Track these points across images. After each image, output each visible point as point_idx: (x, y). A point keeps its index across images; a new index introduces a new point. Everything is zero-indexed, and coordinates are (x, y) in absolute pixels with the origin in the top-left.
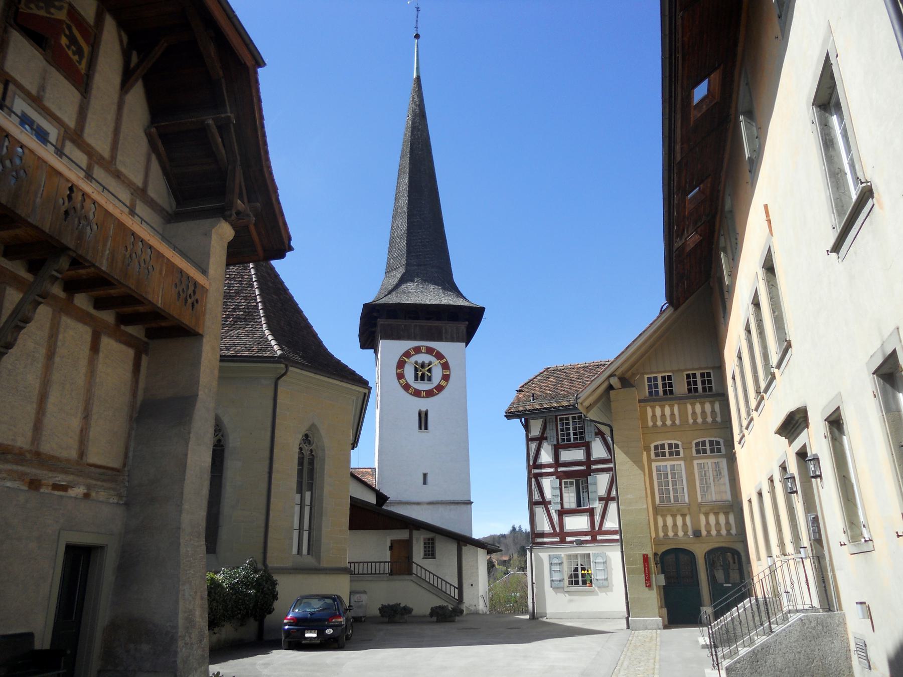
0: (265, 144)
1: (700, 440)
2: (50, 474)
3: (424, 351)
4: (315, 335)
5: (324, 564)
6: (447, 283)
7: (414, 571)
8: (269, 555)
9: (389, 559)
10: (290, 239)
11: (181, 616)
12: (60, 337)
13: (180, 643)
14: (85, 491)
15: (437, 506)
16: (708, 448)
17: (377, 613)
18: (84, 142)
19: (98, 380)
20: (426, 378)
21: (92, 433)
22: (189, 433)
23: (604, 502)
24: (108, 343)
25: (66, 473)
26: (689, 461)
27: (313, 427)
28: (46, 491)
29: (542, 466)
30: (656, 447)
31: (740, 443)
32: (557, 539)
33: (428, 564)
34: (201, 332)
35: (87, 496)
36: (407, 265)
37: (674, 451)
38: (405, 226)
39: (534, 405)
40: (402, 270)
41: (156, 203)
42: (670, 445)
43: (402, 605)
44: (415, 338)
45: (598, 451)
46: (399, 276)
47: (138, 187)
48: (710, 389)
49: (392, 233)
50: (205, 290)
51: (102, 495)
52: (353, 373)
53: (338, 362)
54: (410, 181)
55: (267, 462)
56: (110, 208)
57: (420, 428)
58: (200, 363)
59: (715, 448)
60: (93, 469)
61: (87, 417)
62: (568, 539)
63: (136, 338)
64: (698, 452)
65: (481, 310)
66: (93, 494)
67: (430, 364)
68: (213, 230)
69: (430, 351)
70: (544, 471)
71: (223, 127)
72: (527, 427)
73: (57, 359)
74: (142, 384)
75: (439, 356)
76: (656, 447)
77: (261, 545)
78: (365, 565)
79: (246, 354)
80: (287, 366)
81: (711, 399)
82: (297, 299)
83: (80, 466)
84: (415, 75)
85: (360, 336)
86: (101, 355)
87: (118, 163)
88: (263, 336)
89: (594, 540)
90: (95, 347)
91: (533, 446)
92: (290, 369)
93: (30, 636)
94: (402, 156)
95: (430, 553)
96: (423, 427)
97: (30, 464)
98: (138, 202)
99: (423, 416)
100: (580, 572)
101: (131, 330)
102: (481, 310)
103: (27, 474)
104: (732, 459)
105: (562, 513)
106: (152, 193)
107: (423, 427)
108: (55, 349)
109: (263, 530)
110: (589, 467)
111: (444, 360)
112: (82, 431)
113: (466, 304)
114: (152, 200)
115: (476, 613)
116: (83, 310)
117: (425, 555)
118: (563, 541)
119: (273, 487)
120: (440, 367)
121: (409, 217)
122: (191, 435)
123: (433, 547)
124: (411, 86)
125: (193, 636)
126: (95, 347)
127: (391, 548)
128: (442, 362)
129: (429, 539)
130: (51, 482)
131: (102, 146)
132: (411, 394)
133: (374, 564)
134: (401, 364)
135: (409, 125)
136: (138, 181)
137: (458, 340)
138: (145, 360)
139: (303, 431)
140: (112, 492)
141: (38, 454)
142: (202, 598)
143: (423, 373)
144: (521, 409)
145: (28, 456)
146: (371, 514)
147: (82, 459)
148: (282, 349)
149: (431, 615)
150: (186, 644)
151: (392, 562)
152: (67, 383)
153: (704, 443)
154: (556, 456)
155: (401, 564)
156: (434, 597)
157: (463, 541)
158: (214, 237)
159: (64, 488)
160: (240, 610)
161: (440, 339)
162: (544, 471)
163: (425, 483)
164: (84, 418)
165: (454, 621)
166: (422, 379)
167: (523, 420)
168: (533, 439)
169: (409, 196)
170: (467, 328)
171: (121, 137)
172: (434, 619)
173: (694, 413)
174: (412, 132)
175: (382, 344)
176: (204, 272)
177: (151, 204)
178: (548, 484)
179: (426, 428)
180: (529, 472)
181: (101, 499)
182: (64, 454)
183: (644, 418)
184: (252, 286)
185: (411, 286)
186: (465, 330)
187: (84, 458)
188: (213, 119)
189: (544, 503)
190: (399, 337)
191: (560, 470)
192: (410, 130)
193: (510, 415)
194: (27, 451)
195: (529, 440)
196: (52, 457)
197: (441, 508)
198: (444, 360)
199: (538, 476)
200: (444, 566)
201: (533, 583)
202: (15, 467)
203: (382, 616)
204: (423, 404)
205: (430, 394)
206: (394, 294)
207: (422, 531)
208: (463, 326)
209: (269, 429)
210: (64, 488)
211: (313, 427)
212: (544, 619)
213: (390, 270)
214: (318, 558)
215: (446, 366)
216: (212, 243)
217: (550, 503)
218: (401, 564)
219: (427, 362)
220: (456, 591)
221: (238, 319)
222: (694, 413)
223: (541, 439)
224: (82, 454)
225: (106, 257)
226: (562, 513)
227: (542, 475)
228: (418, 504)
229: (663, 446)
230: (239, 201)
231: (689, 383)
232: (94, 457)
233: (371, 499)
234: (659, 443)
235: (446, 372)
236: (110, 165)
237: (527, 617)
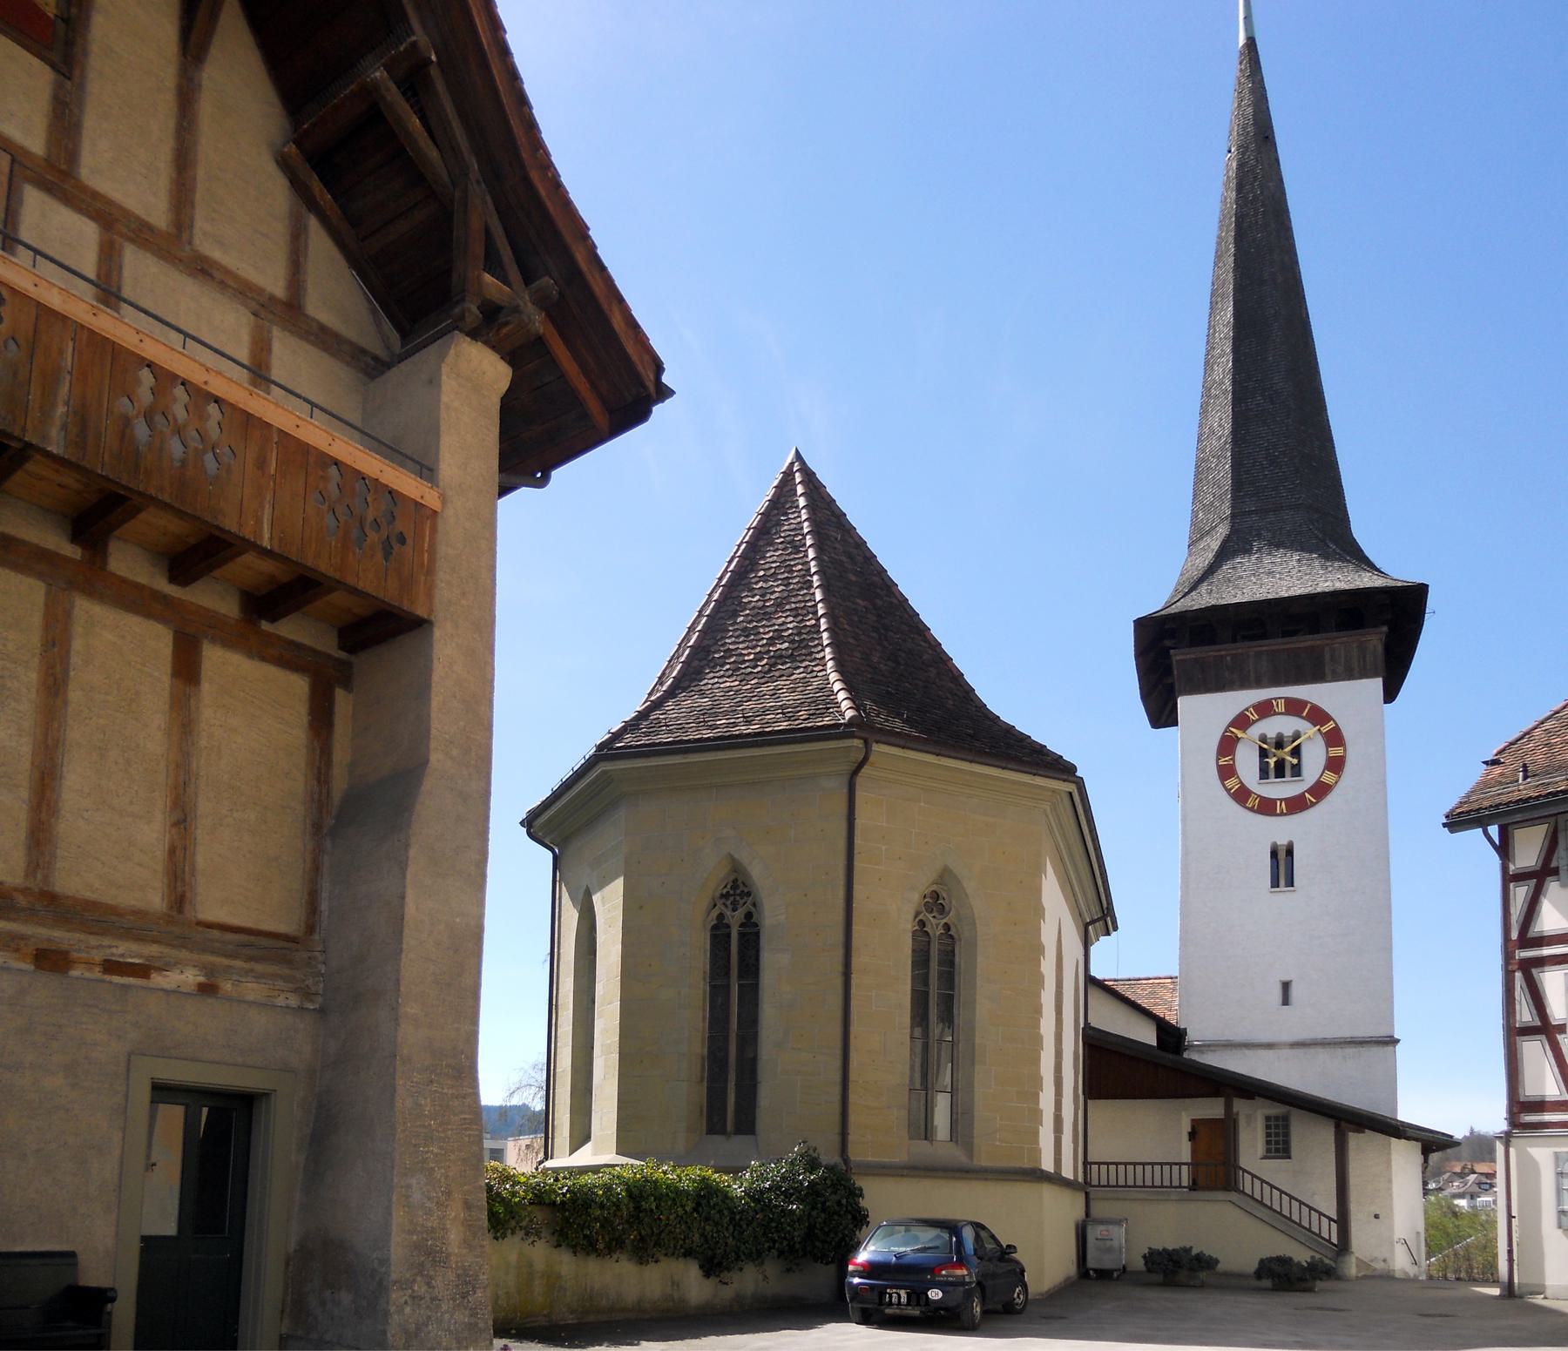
0: (523, 101)
2: (94, 941)
3: (1281, 708)
4: (957, 678)
5: (983, 1160)
6: (1336, 541)
8: (853, 1137)
9: (1186, 1156)
10: (659, 368)
11: (396, 1239)
12: (77, 644)
13: (396, 1296)
15: (1312, 1050)
17: (1139, 1264)
18: (85, 189)
19: (203, 743)
20: (1288, 771)
21: (203, 858)
22: (407, 846)
24: (216, 659)
25: (138, 939)
27: (945, 876)
28: (87, 975)
29: (1542, 941)
33: (1275, 1171)
34: (421, 612)
36: (1233, 516)
38: (1228, 426)
39: (1525, 789)
40: (1223, 530)
41: (337, 336)
43: (1194, 1252)
44: (1258, 683)
46: (1215, 545)
47: (272, 298)
49: (1200, 450)
50: (425, 516)
51: (253, 990)
52: (1040, 750)
53: (1009, 730)
54: (1236, 314)
55: (840, 952)
56: (54, 300)
57: (1275, 883)
58: (428, 687)
60: (216, 933)
61: (182, 818)
63: (314, 651)
65: (1417, 594)
66: (227, 986)
67: (1297, 736)
68: (445, 369)
70: (1547, 951)
71: (414, 82)
72: (1504, 849)
73: (75, 695)
74: (341, 753)
75: (1318, 716)
77: (837, 1118)
78: (1121, 1168)
79: (784, 725)
80: (866, 742)
82: (915, 603)
83: (176, 922)
84: (1242, 40)
85: (1143, 697)
86: (205, 686)
87: (197, 240)
88: (825, 687)
90: (186, 668)
91: (1521, 893)
92: (875, 747)
94: (1219, 256)
95: (1279, 1146)
96: (1282, 882)
97: (45, 923)
98: (276, 332)
99: (1282, 855)
101: (289, 629)
102: (1417, 594)
103: (23, 937)
106: (317, 308)
108: (66, 671)
109: (837, 1089)
111: (1331, 725)
112: (172, 851)
113: (1378, 582)
114: (323, 328)
115: (1388, 1277)
116: (139, 587)
117: (1268, 1151)
119: (853, 1003)
120: (1320, 743)
121: (1236, 402)
122: (412, 853)
124: (1230, 70)
125: (438, 1282)
126: (186, 668)
127: (1192, 1136)
128: (1325, 729)
129: (1277, 1118)
130: (98, 956)
131: (147, 199)
132: (1251, 809)
134: (1227, 745)
135: (1232, 174)
136: (274, 282)
138: (343, 701)
139: (924, 881)
140: (280, 983)
141: (51, 898)
142: (468, 1206)
143: (1280, 760)
144: (1486, 804)
145: (22, 901)
146: (1138, 1063)
147: (180, 911)
148: (857, 707)
149: (1259, 1274)
150: (415, 1298)
151: (1194, 1164)
152: (149, 757)
155: (1214, 1168)
156: (1283, 1237)
157: (1356, 1123)
158: (448, 384)
159: (142, 971)
160: (774, 1242)
161: (1317, 676)
162: (1547, 951)
163: (1286, 1001)
164: (176, 824)
165: (1310, 1290)
166: (1280, 770)
167: (1494, 830)
168: (1520, 877)
169: (1235, 350)
170: (1388, 648)
171: (201, 173)
172: (1267, 1283)
174: (1240, 188)
176: (426, 470)
177: (324, 339)
179: (1290, 883)
180: (1508, 956)
181: (251, 998)
182: (127, 899)
184: (809, 584)
185: (1243, 565)
186: (1380, 648)
187: (187, 907)
188: (387, 68)
190: (1220, 686)
192: (1233, 185)
193: (1457, 821)
194: (16, 889)
195: (1510, 879)
197: (1322, 1055)
198: (1331, 725)
199: (1528, 966)
200: (1307, 1175)
201: (1510, 1217)
203: (1149, 1270)
204: (1281, 829)
205: (1297, 805)
206: (1204, 588)
207: (1259, 1101)
208: (1374, 640)
209: (841, 883)
210: (142, 971)
211: (945, 876)
212: (1538, 1300)
213: (1198, 534)
214: (969, 1148)
215: (1334, 738)
216: (444, 398)
217: (1561, 1028)
218: (1214, 1168)
219: (1288, 733)
220: (1334, 1226)
221: (780, 657)
223: (1541, 876)
224: (179, 900)
225: (58, 423)
227: (1541, 962)
228: (1270, 1046)
230: (488, 278)
232: (212, 905)
233: (1147, 1035)
235: (1336, 751)
236: (174, 245)
237: (1496, 1291)
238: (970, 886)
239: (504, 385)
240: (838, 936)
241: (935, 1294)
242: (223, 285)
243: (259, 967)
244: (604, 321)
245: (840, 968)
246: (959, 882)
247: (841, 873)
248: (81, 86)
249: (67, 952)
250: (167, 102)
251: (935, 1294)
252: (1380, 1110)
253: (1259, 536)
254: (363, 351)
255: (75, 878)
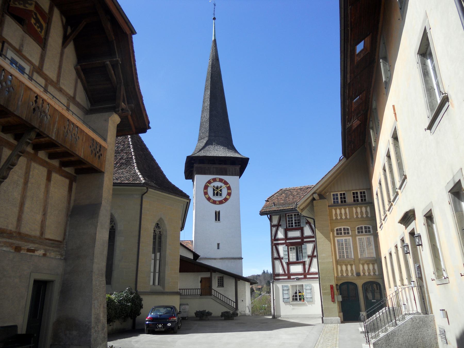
1: (360, 226)
3: (218, 180)
4: (162, 172)
5: (167, 290)
6: (230, 145)
7: (213, 294)
8: (138, 285)
9: (200, 288)
10: (149, 123)
11: (93, 316)
12: (31, 173)
13: (93, 331)
14: (44, 252)
15: (224, 260)
16: (364, 230)
17: (194, 315)
18: (43, 73)
19: (50, 195)
20: (219, 194)
21: (48, 223)
22: (97, 222)
23: (310, 258)
24: (55, 176)
25: (34, 243)
26: (354, 237)
27: (161, 220)
29: (278, 240)
30: (337, 230)
31: (380, 228)
32: (286, 277)
33: (220, 290)
34: (103, 171)
35: (44, 255)
36: (209, 136)
37: (346, 232)
38: (208, 116)
40: (206, 139)
41: (80, 104)
42: (344, 229)
43: (207, 311)
44: (213, 174)
45: (307, 232)
46: (205, 142)
47: (71, 96)
48: (365, 200)
49: (202, 120)
52: (181, 192)
53: (174, 186)
54: (211, 93)
55: (137, 238)
56: (57, 107)
57: (216, 220)
58: (103, 187)
59: (367, 230)
60: (48, 241)
61: (45, 214)
62: (292, 277)
63: (70, 174)
64: (359, 232)
65: (247, 160)
66: (48, 254)
67: (221, 187)
68: (110, 118)
69: (221, 180)
70: (279, 242)
71: (114, 66)
72: (271, 219)
73: (29, 185)
74: (73, 198)
75: (226, 183)
76: (337, 230)
77: (134, 280)
78: (188, 290)
79: (127, 182)
80: (147, 188)
81: (365, 205)
83: (41, 240)
84: (213, 39)
85: (185, 173)
86: (52, 182)
88: (135, 173)
89: (305, 278)
90: (49, 179)
91: (274, 229)
92: (149, 189)
93: (15, 327)
94: (207, 80)
95: (221, 284)
96: (217, 220)
97: (16, 239)
98: (71, 104)
99: (217, 214)
100: (298, 294)
101: (67, 169)
102: (247, 160)
104: (376, 236)
105: (289, 264)
106: (78, 99)
107: (217, 220)
108: (28, 179)
110: (302, 240)
111: (228, 185)
112: (42, 221)
113: (239, 156)
114: (78, 103)
115: (245, 315)
117: (218, 285)
118: (289, 278)
120: (226, 189)
122: (98, 224)
123: (222, 281)
124: (211, 44)
125: (99, 327)
126: (49, 179)
127: (201, 282)
128: (227, 186)
129: (220, 277)
130: (26, 248)
131: (52, 75)
132: (211, 202)
133: (192, 290)
134: (206, 187)
136: (71, 93)
137: (236, 175)
138: (74, 185)
139: (156, 221)
140: (57, 253)
141: (19, 233)
142: (104, 308)
143: (217, 192)
146: (191, 264)
147: (42, 236)
148: (145, 179)
149: (222, 316)
152: (34, 197)
153: (362, 228)
154: (286, 234)
155: (206, 290)
156: (223, 307)
159: (33, 251)
160: (123, 313)
161: (226, 174)
162: (279, 242)
163: (218, 248)
165: (233, 319)
166: (217, 195)
167: (269, 216)
168: (274, 226)
169: (210, 101)
170: (240, 169)
172: (223, 318)
173: (357, 212)
174: (212, 68)
175: (196, 177)
176: (105, 140)
177: (78, 105)
178: (282, 249)
179: (219, 220)
180: (272, 242)
182: (33, 233)
183: (331, 215)
184: (130, 147)
186: (239, 170)
188: (109, 61)
189: (280, 258)
190: (205, 173)
191: (288, 241)
192: (210, 67)
193: (262, 213)
195: (272, 226)
196: (27, 235)
197: (227, 261)
198: (228, 185)
200: (228, 291)
201: (274, 300)
202: (8, 240)
203: (196, 317)
204: (217, 208)
205: (221, 202)
206: (202, 151)
207: (217, 273)
208: (238, 168)
209: (138, 221)
210: (33, 251)
211: (161, 220)
212: (280, 318)
213: (200, 139)
214: (164, 287)
215: (229, 188)
216: (109, 125)
217: (282, 258)
218: (206, 290)
219: (219, 186)
220: (235, 304)
221: (122, 164)
222: (357, 212)
223: (278, 226)
224: (42, 233)
226: (289, 264)
227: (278, 244)
228: (215, 259)
229: (340, 229)
230: (123, 104)
231: (354, 197)
232: (48, 235)
233: (191, 256)
234: (338, 228)
236: (56, 85)
237: (271, 317)
238: (166, 222)
239: (119, 122)
240: (137, 233)
241: (169, 325)
242: (63, 93)
243: (54, 249)
244: (142, 114)
245: (137, 241)
246: (163, 221)
247: (138, 218)
248: (45, 53)
249: (20, 247)
250: (59, 55)
251: (169, 325)
252: (240, 275)
253: (215, 142)
254: (84, 108)
255: (25, 229)
